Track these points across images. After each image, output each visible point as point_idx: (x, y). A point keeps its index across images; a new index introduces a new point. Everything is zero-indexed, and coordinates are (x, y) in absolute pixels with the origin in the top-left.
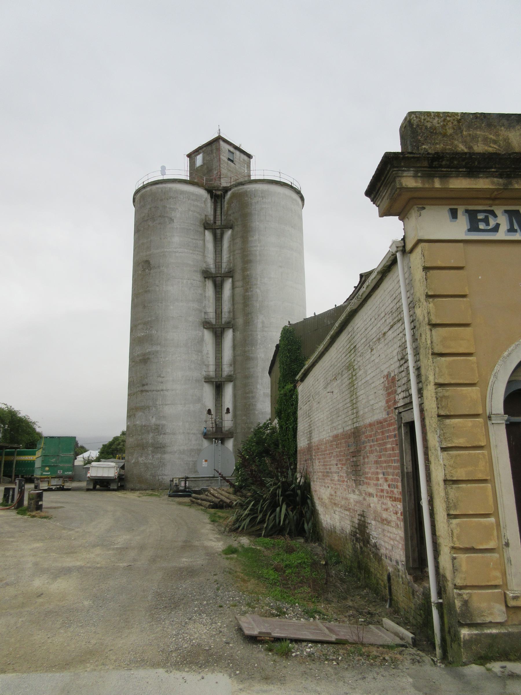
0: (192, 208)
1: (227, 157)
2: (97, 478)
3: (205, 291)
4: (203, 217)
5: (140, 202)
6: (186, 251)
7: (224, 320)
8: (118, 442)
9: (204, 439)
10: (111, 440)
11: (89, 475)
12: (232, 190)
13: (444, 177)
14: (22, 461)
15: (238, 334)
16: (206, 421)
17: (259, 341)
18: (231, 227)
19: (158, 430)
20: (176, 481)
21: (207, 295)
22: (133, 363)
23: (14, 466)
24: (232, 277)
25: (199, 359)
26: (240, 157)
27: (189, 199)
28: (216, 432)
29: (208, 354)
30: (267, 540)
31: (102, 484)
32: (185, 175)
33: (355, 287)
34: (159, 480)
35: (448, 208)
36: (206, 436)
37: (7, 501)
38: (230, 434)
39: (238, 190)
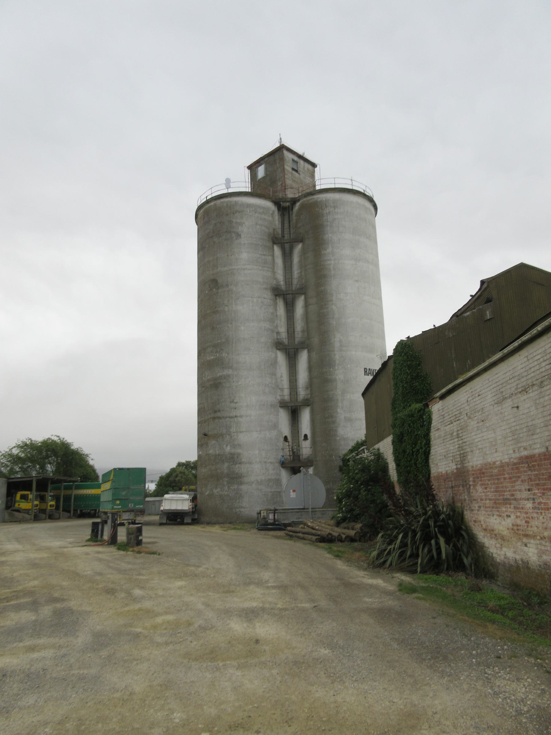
0: (260, 222)
1: (292, 166)
2: (170, 511)
3: (276, 310)
4: (271, 231)
5: (204, 218)
6: (253, 268)
7: (297, 340)
8: (175, 474)
9: (281, 468)
10: (168, 470)
11: (162, 508)
12: (301, 201)
14: (81, 495)
15: (314, 355)
16: (283, 449)
17: (337, 362)
18: (302, 241)
19: (234, 459)
20: (263, 514)
21: (278, 314)
22: (203, 389)
23: (73, 501)
24: (304, 294)
25: (273, 382)
26: (304, 167)
27: (256, 213)
28: (294, 460)
29: (281, 377)
31: (175, 518)
32: (246, 187)
33: (471, 296)
34: (236, 513)
36: (283, 464)
37: (97, 537)
38: (309, 463)
39: (307, 201)
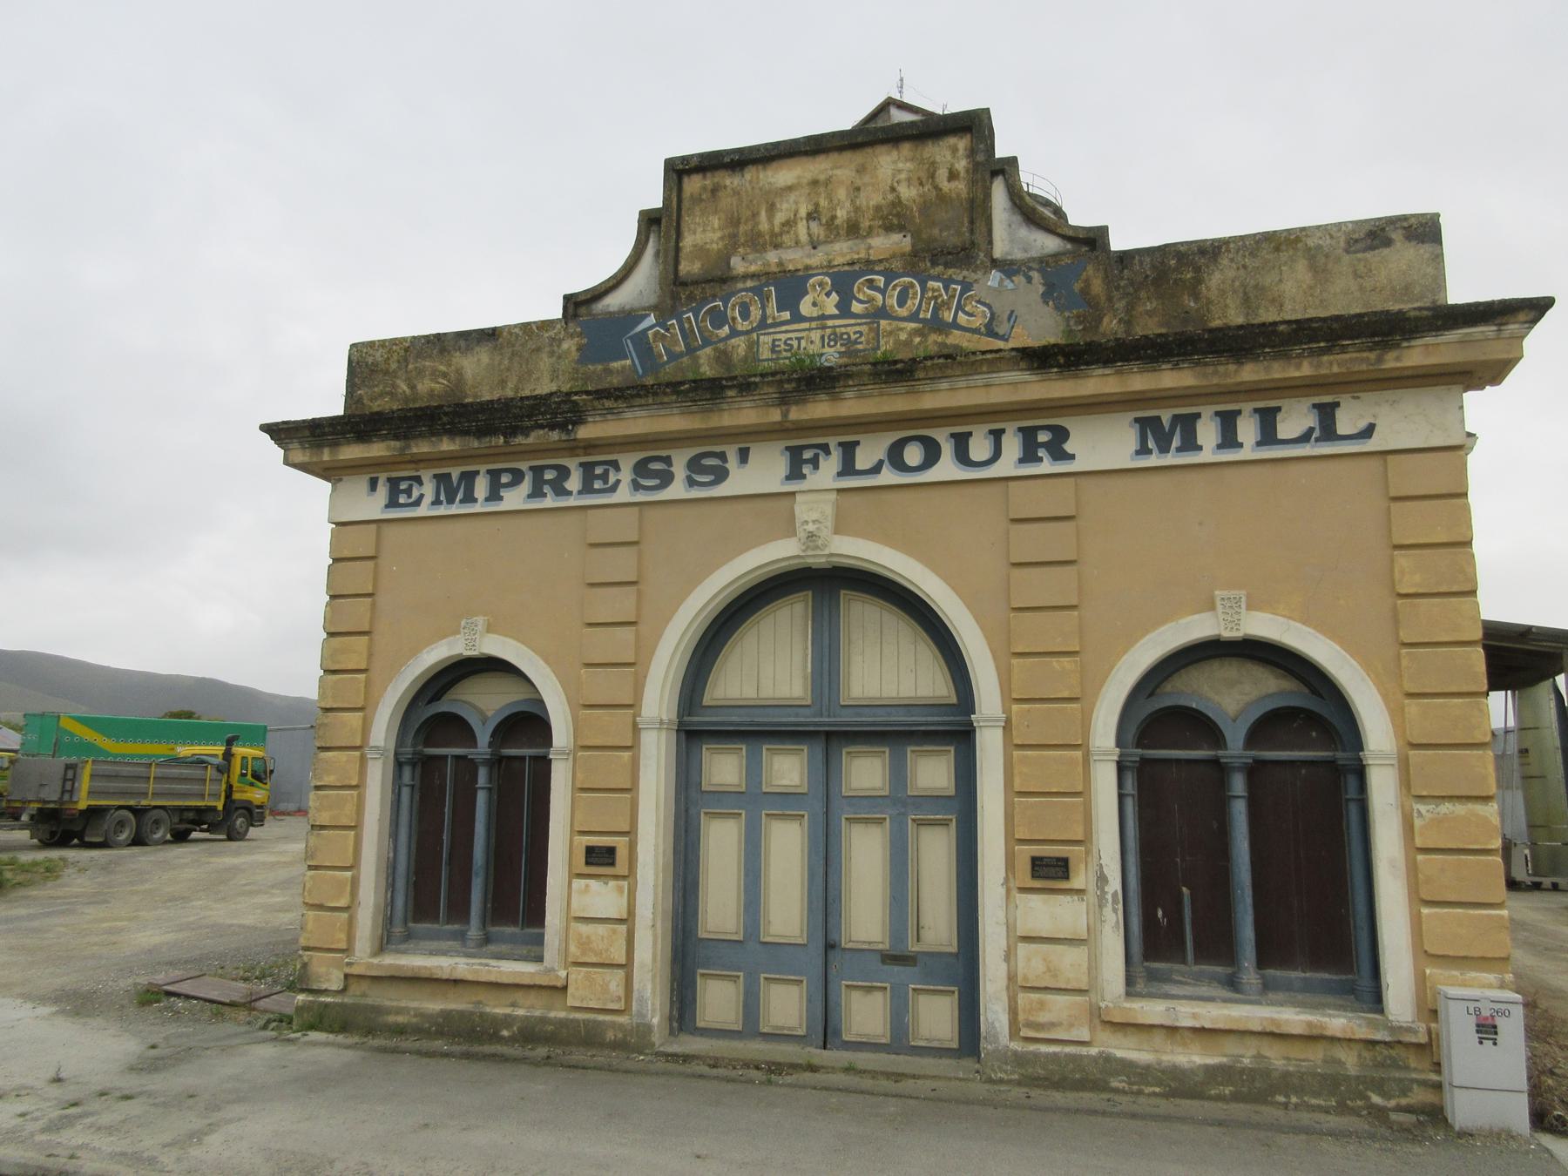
13: (335, 445)
30: (1196, 968)
35: (368, 477)
